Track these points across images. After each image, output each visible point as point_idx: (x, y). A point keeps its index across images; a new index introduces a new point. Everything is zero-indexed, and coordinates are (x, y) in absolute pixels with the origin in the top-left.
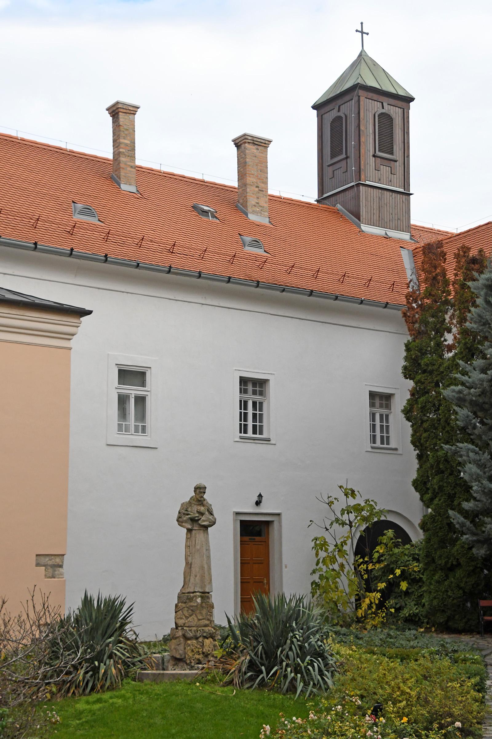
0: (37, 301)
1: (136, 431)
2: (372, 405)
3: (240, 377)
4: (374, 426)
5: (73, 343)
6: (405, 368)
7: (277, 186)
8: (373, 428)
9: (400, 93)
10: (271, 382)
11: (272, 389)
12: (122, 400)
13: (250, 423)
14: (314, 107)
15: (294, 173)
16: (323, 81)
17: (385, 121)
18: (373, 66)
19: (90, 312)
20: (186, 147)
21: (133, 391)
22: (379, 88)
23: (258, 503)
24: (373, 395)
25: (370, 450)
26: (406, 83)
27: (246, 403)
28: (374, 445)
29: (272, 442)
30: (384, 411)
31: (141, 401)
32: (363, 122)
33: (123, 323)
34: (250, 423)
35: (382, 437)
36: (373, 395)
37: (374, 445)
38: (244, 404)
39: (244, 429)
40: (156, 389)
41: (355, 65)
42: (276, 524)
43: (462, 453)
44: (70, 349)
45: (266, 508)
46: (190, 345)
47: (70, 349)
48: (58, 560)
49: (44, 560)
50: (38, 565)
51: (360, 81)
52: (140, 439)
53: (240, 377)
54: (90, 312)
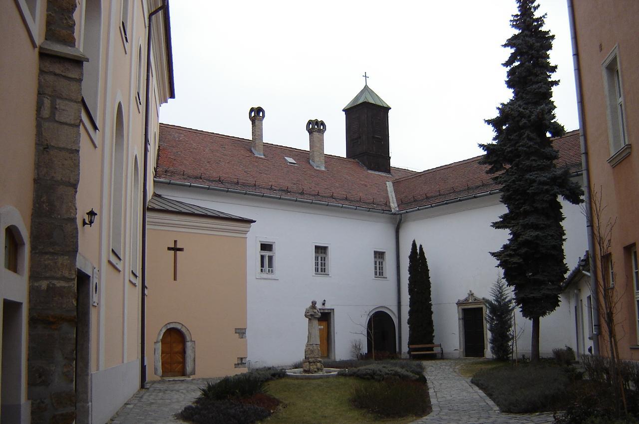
0: (233, 217)
1: (269, 272)
2: (375, 257)
3: (374, 251)
4: (376, 267)
5: (248, 235)
6: (550, 47)
7: (328, 150)
8: (376, 267)
9: (384, 106)
10: (329, 248)
11: (276, 248)
12: (262, 257)
13: (320, 267)
14: (343, 110)
15: (336, 143)
16: (347, 98)
17: (376, 275)
18: (371, 93)
19: (255, 221)
20: (285, 132)
21: (267, 254)
22: (374, 103)
23: (324, 304)
24: (376, 253)
25: (374, 278)
26: (387, 100)
27: (317, 257)
28: (376, 276)
29: (330, 276)
30: (381, 260)
31: (270, 258)
32: (368, 121)
33: (272, 223)
34: (320, 267)
35: (380, 272)
36: (376, 253)
37: (376, 276)
38: (317, 258)
39: (317, 270)
40: (278, 253)
41: (362, 92)
42: (332, 314)
43: (578, 370)
44: (246, 238)
45: (328, 306)
46: (290, 231)
47: (246, 238)
48: (244, 331)
49: (238, 331)
50: (236, 333)
51: (366, 100)
52: (270, 276)
53: (374, 251)
54: (255, 221)
